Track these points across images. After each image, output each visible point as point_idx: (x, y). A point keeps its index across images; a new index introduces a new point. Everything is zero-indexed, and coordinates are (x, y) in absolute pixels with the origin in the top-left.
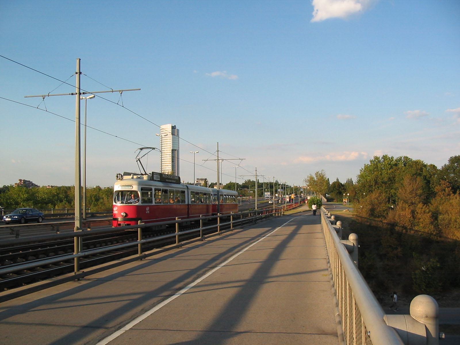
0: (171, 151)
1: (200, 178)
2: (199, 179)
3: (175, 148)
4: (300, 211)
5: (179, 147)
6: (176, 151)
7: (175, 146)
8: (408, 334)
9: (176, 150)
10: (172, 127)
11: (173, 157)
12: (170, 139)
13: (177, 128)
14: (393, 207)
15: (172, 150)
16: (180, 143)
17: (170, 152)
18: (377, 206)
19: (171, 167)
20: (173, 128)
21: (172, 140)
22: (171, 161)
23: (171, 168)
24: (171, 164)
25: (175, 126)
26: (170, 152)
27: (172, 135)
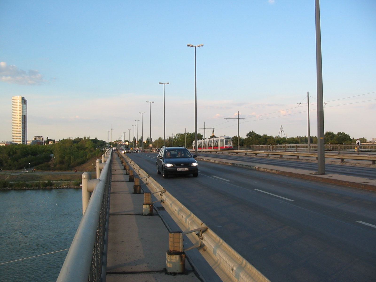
0: (21, 116)
1: (37, 136)
2: (36, 136)
3: (24, 114)
4: (189, 45)
5: (27, 107)
6: (25, 116)
7: (24, 112)
8: (93, 187)
9: (25, 115)
10: (22, 98)
11: (23, 138)
12: (20, 140)
13: (25, 99)
14: (128, 144)
15: (22, 115)
16: (27, 113)
17: (21, 130)
18: (56, 185)
19: (21, 128)
20: (23, 99)
21: (22, 108)
22: (21, 124)
23: (21, 129)
24: (21, 126)
25: (24, 97)
26: (21, 127)
27: (22, 104)
